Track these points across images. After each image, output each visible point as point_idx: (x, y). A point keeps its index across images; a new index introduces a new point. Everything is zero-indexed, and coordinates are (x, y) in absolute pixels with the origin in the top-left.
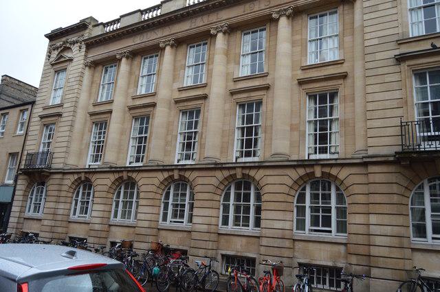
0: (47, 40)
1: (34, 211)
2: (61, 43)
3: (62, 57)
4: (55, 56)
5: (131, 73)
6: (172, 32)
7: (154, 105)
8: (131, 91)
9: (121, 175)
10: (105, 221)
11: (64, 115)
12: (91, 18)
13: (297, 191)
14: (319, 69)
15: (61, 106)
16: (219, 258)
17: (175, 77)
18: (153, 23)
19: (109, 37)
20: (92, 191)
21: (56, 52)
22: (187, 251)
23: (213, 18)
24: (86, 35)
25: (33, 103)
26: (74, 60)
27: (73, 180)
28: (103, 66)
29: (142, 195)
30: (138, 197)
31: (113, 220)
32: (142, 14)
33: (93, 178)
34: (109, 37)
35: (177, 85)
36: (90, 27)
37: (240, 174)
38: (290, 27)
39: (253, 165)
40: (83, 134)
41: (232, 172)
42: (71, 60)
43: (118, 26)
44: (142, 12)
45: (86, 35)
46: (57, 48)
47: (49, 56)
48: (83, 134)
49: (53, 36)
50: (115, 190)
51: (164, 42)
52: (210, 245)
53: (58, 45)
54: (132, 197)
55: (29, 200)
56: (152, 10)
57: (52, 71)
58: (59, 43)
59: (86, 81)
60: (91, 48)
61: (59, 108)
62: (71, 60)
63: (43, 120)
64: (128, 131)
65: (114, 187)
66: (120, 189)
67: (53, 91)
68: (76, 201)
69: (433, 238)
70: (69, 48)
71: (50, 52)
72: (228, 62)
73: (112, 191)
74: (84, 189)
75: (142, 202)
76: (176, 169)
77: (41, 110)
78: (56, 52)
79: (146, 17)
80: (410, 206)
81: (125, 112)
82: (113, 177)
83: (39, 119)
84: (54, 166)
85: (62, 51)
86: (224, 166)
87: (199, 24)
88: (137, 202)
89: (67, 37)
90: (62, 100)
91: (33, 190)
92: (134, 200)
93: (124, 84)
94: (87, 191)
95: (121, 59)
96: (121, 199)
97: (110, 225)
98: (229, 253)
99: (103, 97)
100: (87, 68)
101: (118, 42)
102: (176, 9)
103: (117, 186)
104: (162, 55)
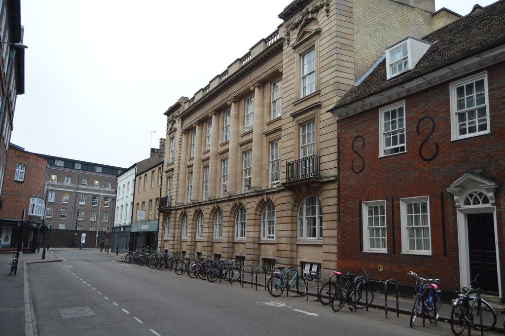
0: (166, 116)
1: (242, 236)
2: (300, 17)
3: (305, 33)
4: (295, 36)
5: (201, 135)
6: (252, 79)
13: (298, 207)
14: (273, 124)
15: (318, 93)
18: (268, 53)
20: (317, 206)
21: (297, 31)
22: (221, 255)
24: (181, 110)
25: (163, 163)
26: (324, 30)
27: (257, 202)
28: (271, 83)
29: (325, 210)
30: (321, 212)
31: (264, 239)
32: (266, 42)
33: (221, 205)
35: (220, 142)
36: (183, 104)
39: (241, 196)
40: (185, 181)
42: (318, 32)
43: (250, 58)
44: (265, 41)
45: (181, 110)
46: (297, 26)
49: (168, 113)
50: (261, 212)
51: (253, 85)
53: (297, 20)
54: (314, 213)
55: (299, 221)
56: (270, 39)
57: (296, 55)
58: (297, 18)
61: (171, 166)
62: (318, 32)
63: (297, 119)
64: (220, 170)
66: (265, 210)
67: (302, 80)
69: (244, 236)
70: (313, 19)
71: (168, 125)
74: (241, 213)
75: (325, 217)
78: (297, 31)
79: (269, 43)
80: (298, 217)
82: (257, 200)
83: (291, 118)
84: (323, 174)
85: (302, 27)
88: (321, 218)
89: (174, 114)
90: (317, 87)
91: (238, 215)
92: (317, 216)
93: (229, 129)
95: (254, 90)
97: (196, 242)
98: (217, 253)
100: (183, 135)
101: (188, 119)
102: (258, 54)
104: (195, 132)
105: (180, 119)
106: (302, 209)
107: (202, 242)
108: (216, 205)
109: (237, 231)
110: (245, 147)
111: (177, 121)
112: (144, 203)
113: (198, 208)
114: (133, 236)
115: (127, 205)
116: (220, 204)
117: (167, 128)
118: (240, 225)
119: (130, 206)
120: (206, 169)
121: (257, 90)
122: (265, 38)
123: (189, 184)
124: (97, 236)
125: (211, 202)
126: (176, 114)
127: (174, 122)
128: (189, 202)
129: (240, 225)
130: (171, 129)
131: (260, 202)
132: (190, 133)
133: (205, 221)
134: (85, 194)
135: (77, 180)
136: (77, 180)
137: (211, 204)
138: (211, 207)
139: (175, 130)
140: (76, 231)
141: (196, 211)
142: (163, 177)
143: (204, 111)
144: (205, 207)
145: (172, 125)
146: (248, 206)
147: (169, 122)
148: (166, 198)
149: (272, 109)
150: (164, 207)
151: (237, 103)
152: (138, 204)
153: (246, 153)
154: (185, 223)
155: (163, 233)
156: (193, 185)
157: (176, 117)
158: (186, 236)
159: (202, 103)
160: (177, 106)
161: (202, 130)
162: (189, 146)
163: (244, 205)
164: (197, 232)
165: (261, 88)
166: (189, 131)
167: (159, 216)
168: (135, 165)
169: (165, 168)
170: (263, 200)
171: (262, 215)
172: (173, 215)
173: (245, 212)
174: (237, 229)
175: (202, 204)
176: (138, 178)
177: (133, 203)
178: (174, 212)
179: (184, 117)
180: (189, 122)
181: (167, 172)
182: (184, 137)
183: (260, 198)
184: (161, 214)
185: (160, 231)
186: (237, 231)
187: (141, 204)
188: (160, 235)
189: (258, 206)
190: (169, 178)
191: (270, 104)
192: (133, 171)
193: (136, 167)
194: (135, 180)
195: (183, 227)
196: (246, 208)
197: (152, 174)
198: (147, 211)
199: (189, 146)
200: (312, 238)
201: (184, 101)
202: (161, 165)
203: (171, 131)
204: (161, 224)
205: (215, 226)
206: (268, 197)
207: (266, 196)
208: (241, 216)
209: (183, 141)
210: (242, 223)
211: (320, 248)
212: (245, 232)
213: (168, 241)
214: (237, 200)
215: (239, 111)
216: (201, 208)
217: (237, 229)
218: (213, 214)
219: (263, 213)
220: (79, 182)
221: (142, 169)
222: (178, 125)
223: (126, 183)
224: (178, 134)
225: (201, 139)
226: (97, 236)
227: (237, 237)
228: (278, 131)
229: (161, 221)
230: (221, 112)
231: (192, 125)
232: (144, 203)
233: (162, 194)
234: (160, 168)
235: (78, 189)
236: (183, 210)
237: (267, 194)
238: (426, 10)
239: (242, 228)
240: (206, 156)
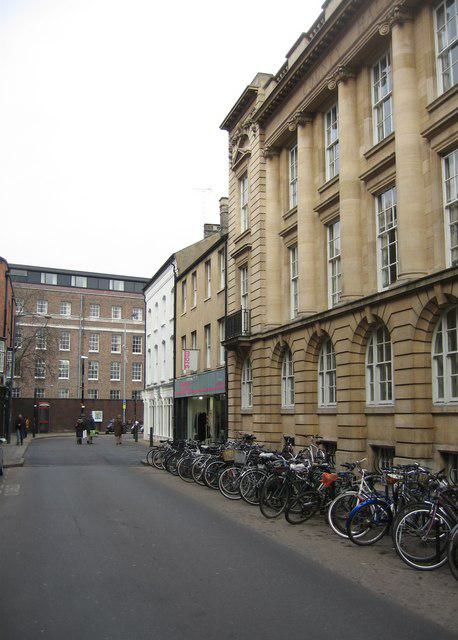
1: (383, 398)
5: (312, 148)
7: (391, 162)
8: (317, 180)
9: (431, 296)
10: (421, 406)
11: (254, 247)
12: (260, 75)
16: (437, 456)
17: (359, 140)
19: (342, 19)
23: (367, 20)
34: (278, 100)
35: (364, 149)
37: (440, 295)
38: (407, 42)
40: (280, 271)
41: (431, 296)
45: (257, 105)
47: (231, 152)
48: (280, 271)
49: (229, 124)
50: (430, 332)
51: (333, 79)
52: (418, 436)
55: (435, 364)
59: (270, 183)
60: (267, 125)
64: (370, 221)
65: (426, 326)
66: (372, 343)
68: (439, 359)
69: (390, 398)
72: (417, 78)
73: (423, 336)
74: (380, 340)
76: (366, 305)
77: (233, 246)
81: (314, 220)
86: (418, 286)
87: (351, 42)
91: (322, 358)
93: (342, 146)
94: (384, 343)
95: (390, 32)
96: (376, 362)
99: (422, 94)
103: (433, 323)
105: (257, 127)
106: (439, 337)
107: (335, 415)
108: (368, 314)
109: (372, 385)
110: (328, 211)
111: (250, 134)
112: (194, 333)
113: (317, 328)
114: (180, 403)
115: (164, 343)
116: (382, 309)
117: (230, 158)
118: (377, 372)
119: (170, 344)
120: (294, 251)
121: (341, 89)
122: (306, 31)
123: (289, 275)
124: (124, 407)
125: (306, 323)
126: (247, 118)
127: (245, 138)
128: (293, 316)
129: (379, 370)
130: (239, 154)
131: (312, 339)
132: (284, 153)
133: (298, 366)
134: (98, 333)
135: (83, 308)
136: (83, 308)
137: (353, 312)
138: (353, 322)
139: (248, 155)
140: (83, 400)
141: (314, 337)
142: (229, 270)
143: (315, 83)
144: (295, 336)
145: (241, 145)
146: (397, 320)
147: (233, 142)
148: (238, 314)
149: (291, 193)
150: (238, 342)
151: (351, 82)
152: (184, 338)
153: (330, 225)
154: (287, 370)
155: (238, 398)
156: (300, 276)
157: (247, 128)
158: (293, 402)
159: (273, 110)
160: (250, 95)
161: (279, 166)
162: (283, 185)
163: (385, 320)
164: (283, 395)
165: (351, 82)
166: (282, 147)
167: (226, 360)
168: (172, 258)
169: (232, 248)
170: (364, 320)
171: (433, 343)
172: (255, 355)
173: (388, 339)
174: (372, 380)
175: (326, 318)
176: (179, 284)
177: (174, 338)
178: (258, 345)
179: (264, 120)
180: (275, 128)
181: (236, 256)
182: (269, 168)
183: (358, 318)
184: (230, 354)
185: (231, 394)
186: (372, 385)
187: (189, 337)
188: (231, 402)
189: (309, 345)
190: (244, 267)
191: (288, 187)
192: (169, 273)
193: (175, 263)
194: (175, 290)
195: (283, 383)
196: (390, 328)
197: (206, 267)
198: (202, 350)
199: (282, 185)
200: (383, 402)
201: (263, 84)
202: (224, 245)
203: (239, 162)
204: (231, 377)
205: (320, 378)
206: (374, 312)
207: (371, 311)
208: (380, 349)
209: (268, 176)
210: (381, 366)
211: (387, 421)
212: (390, 389)
213: (393, 414)
214: (280, 337)
215: (414, 45)
216: (326, 327)
217: (372, 380)
218: (277, 359)
219: (368, 349)
220: (85, 313)
221: (186, 268)
222: (254, 145)
223: (160, 298)
224: (254, 165)
225: (312, 159)
226: (124, 407)
227: (441, 394)
228: (380, 173)
229: (231, 369)
230: (360, 72)
231: (326, 89)
232: (194, 333)
233: (230, 308)
234: (220, 252)
235: (84, 323)
236: (280, 338)
237: (372, 306)
238: (80, 374)
239: (383, 377)
240: (290, 223)
